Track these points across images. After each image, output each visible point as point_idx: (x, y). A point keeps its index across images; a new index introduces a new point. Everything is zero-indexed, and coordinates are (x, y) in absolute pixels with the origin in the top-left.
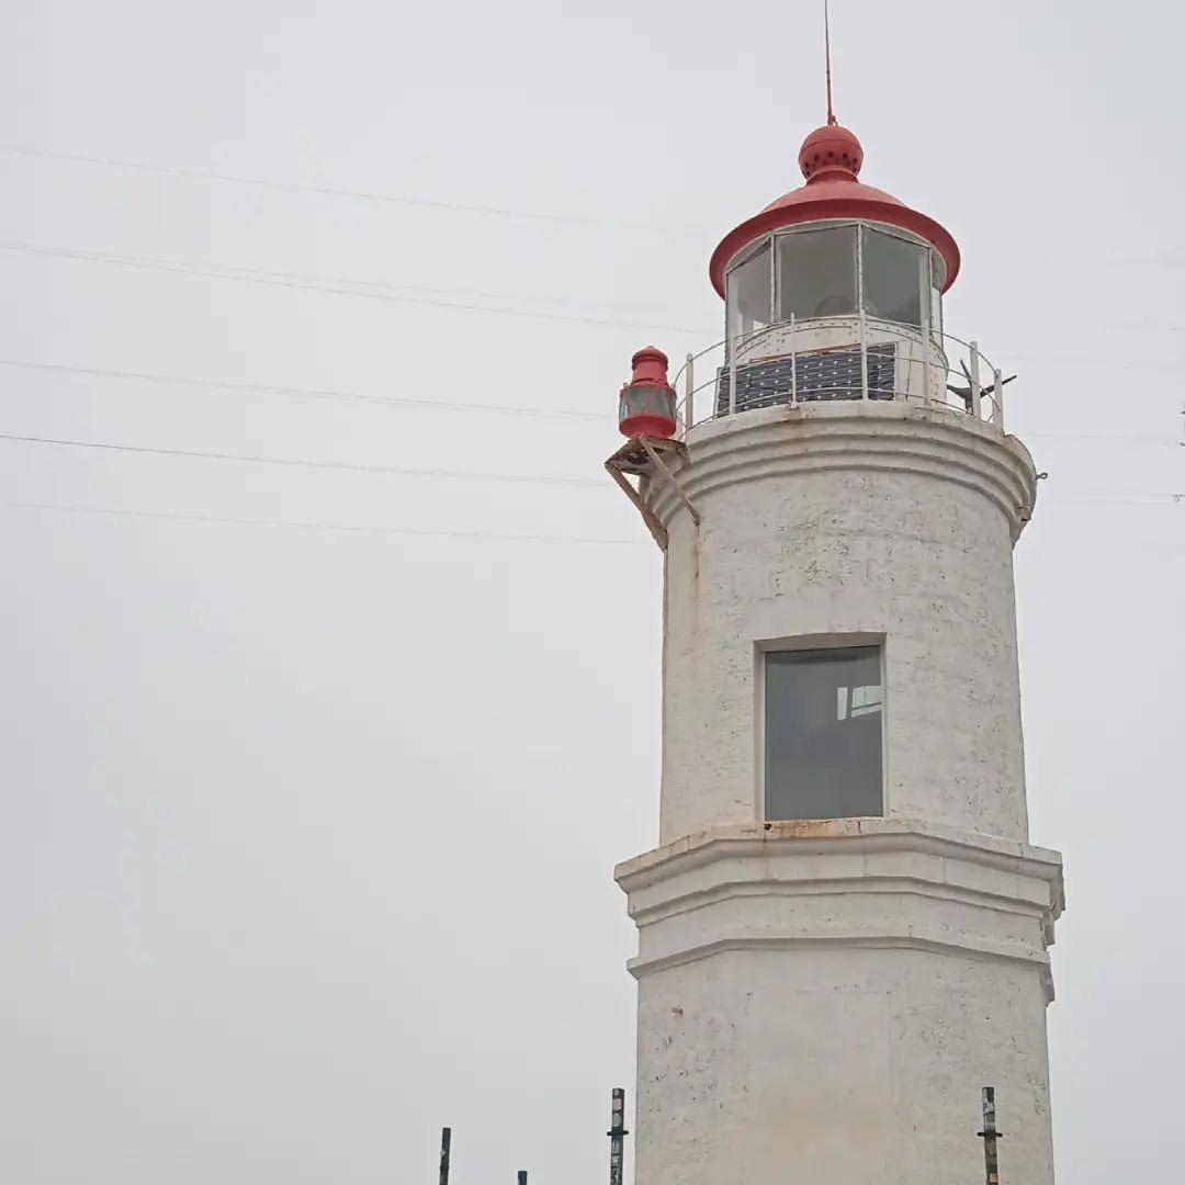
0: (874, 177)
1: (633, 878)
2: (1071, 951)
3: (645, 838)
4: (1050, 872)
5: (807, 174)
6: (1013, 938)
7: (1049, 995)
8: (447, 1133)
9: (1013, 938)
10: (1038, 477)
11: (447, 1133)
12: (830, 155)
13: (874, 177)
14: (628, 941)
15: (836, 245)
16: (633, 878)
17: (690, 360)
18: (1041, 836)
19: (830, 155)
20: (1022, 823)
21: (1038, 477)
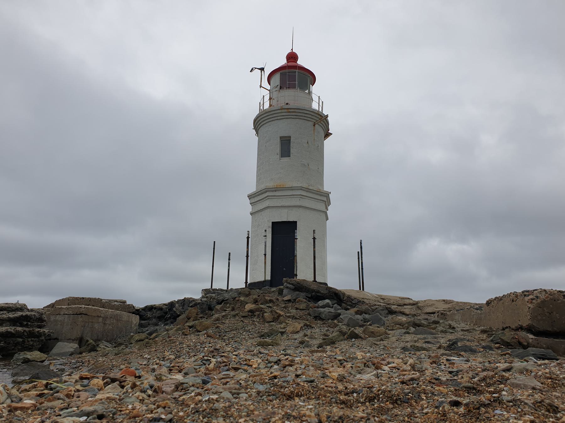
0: (300, 62)
1: (250, 197)
2: (331, 211)
3: (253, 189)
4: (327, 195)
5: (287, 60)
6: (321, 207)
7: (327, 219)
8: (230, 253)
9: (321, 207)
10: (315, 281)
11: (230, 253)
12: (292, 57)
13: (300, 62)
14: (250, 208)
15: (293, 76)
16: (250, 197)
17: (264, 96)
18: (326, 188)
19: (292, 57)
20: (322, 185)
21: (315, 281)
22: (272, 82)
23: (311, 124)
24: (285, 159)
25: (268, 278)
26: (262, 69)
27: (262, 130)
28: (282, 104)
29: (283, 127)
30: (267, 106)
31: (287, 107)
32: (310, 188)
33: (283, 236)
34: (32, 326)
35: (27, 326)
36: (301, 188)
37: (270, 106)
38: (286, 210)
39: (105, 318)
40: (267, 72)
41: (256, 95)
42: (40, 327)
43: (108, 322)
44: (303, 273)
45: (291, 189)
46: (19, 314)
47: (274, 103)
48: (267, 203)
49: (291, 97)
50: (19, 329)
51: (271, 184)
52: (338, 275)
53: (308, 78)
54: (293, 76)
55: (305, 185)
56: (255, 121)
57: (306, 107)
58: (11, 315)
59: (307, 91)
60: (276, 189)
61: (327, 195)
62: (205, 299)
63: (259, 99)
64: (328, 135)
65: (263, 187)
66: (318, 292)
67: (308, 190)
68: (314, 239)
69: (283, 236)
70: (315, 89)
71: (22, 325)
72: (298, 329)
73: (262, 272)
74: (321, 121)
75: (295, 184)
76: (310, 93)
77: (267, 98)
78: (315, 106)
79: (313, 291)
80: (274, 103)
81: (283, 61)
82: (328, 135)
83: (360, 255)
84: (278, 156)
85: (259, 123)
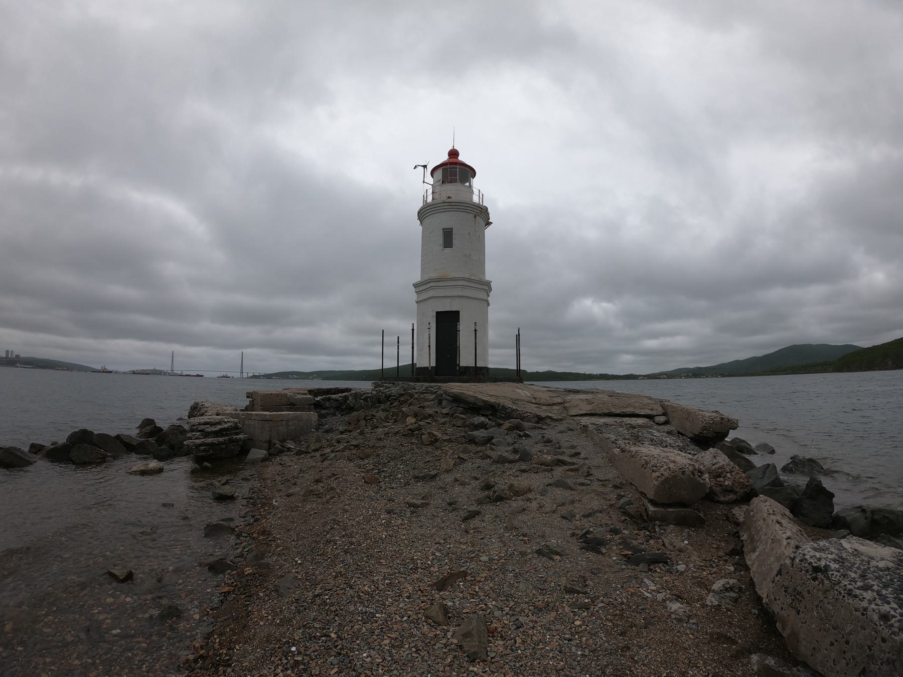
0: (461, 158)
3: (417, 278)
6: (482, 295)
9: (482, 295)
12: (454, 154)
14: (415, 297)
15: (454, 171)
16: (416, 286)
18: (488, 277)
19: (454, 154)
20: (484, 273)
22: (435, 175)
23: (472, 216)
24: (448, 250)
25: (433, 364)
26: (425, 167)
27: (426, 221)
28: (444, 198)
29: (445, 220)
30: (430, 199)
31: (449, 200)
32: (473, 278)
33: (447, 324)
34: (231, 434)
35: (227, 435)
36: (464, 279)
37: (433, 199)
38: (449, 300)
39: (288, 421)
40: (430, 168)
41: (419, 188)
42: (237, 434)
43: (290, 423)
44: (466, 360)
45: (454, 279)
46: (219, 427)
47: (437, 196)
48: (431, 293)
49: (452, 190)
50: (221, 439)
51: (434, 275)
52: (498, 357)
53: (468, 172)
54: (454, 171)
55: (467, 276)
56: (419, 213)
57: (467, 200)
58: (213, 429)
59: (467, 184)
60: (439, 280)
61: (488, 284)
62: (374, 393)
63: (423, 193)
64: (488, 224)
65: (427, 277)
66: (475, 404)
67: (470, 280)
68: (476, 330)
69: (447, 324)
70: (476, 183)
71: (223, 436)
72: (451, 466)
73: (427, 359)
74: (481, 214)
75: (458, 275)
76: (470, 186)
77: (430, 192)
78: (476, 199)
79: (469, 403)
80: (437, 196)
81: (445, 158)
82: (488, 224)
83: (518, 337)
84: (441, 247)
85: (424, 214)
